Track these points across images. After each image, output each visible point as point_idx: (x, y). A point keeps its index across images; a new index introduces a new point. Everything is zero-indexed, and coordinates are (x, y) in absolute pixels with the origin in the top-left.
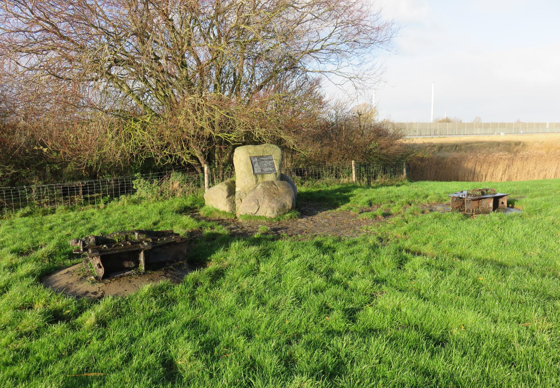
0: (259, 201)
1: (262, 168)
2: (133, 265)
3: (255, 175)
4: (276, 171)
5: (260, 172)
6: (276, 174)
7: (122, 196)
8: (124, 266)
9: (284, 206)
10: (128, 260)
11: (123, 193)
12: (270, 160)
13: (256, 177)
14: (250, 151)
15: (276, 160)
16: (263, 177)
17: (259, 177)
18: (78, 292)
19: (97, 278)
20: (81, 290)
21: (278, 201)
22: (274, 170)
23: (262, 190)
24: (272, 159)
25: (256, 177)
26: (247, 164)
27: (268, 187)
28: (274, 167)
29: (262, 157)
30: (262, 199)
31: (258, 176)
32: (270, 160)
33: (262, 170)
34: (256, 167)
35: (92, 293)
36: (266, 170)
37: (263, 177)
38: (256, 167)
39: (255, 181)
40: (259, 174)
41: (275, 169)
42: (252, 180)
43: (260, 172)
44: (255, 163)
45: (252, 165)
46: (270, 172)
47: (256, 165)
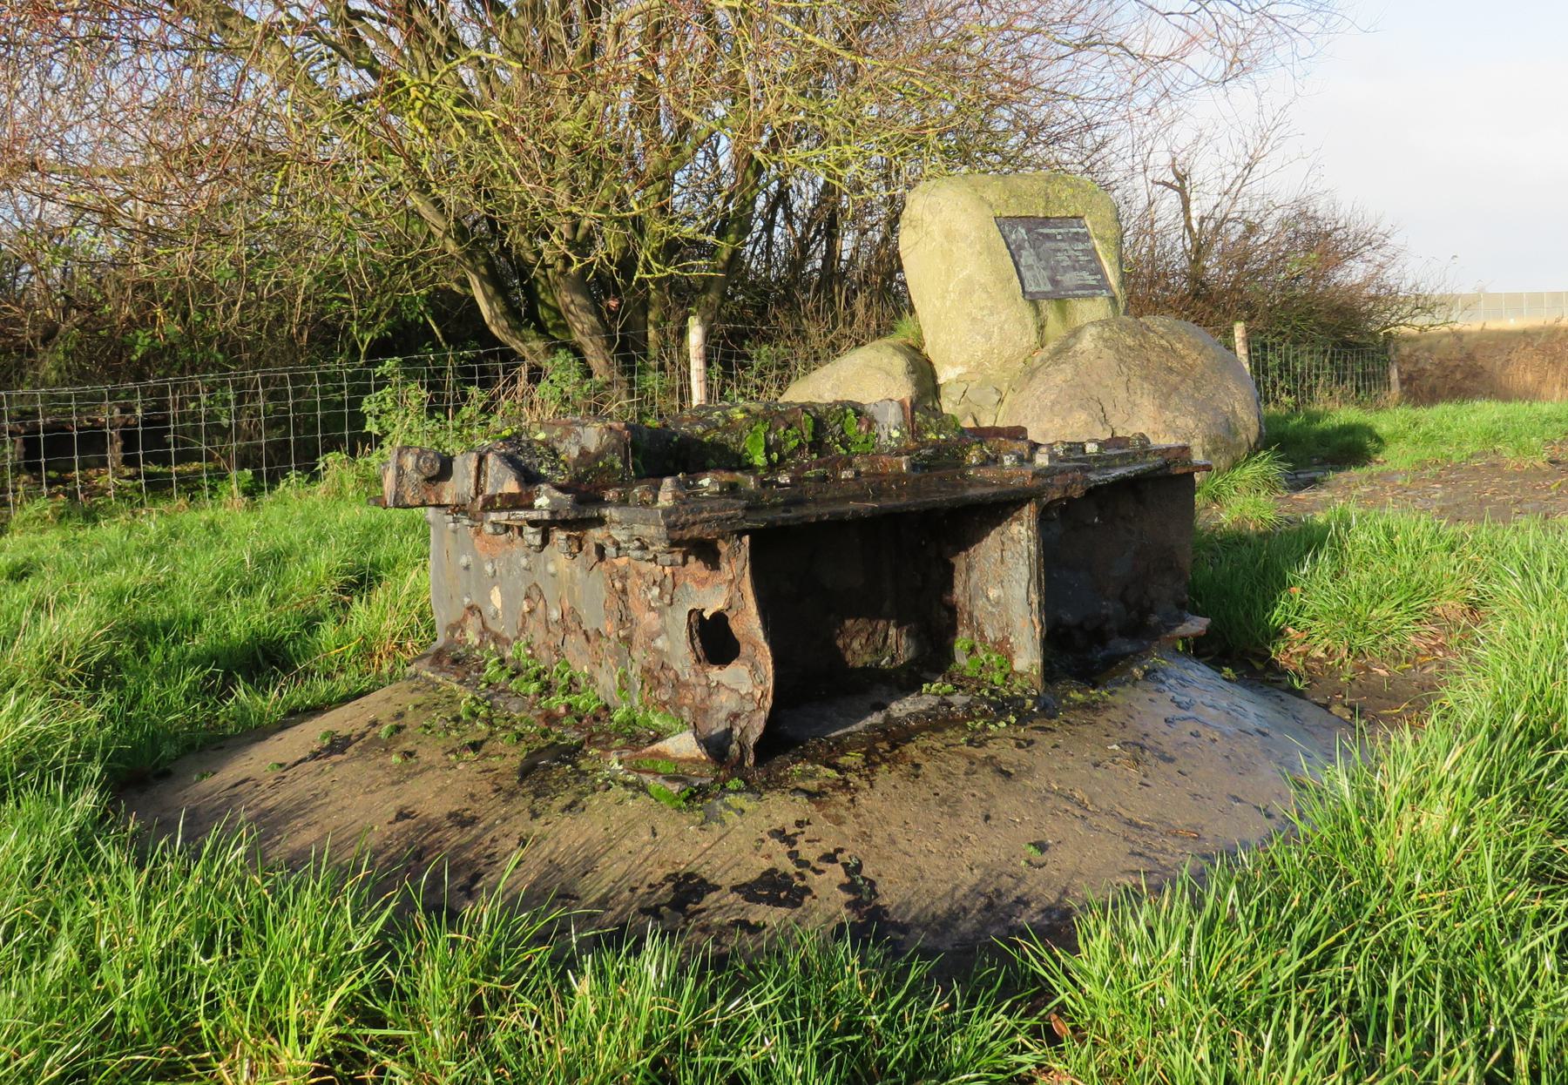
0: (1109, 408)
1: (1054, 270)
2: (899, 645)
3: (1033, 300)
4: (1109, 288)
5: (1049, 288)
6: (1113, 299)
7: (330, 457)
8: (838, 656)
9: (1230, 429)
10: (871, 610)
11: (332, 445)
12: (1077, 237)
13: (1038, 312)
14: (990, 196)
15: (1102, 239)
16: (1063, 312)
17: (1050, 311)
18: (593, 888)
19: (717, 747)
20: (611, 872)
21: (1201, 407)
22: (1103, 284)
23: (1108, 354)
24: (1087, 237)
25: (1038, 312)
26: (989, 248)
27: (1130, 341)
28: (1099, 270)
29: (1046, 220)
30: (1121, 394)
31: (1044, 304)
32: (1077, 237)
33: (1054, 282)
34: (1030, 267)
35: (749, 891)
36: (1070, 279)
37: (1063, 312)
38: (1030, 267)
39: (1032, 328)
40: (1046, 295)
41: (1104, 277)
42: (1021, 321)
43: (1049, 288)
44: (1020, 247)
45: (1013, 256)
46: (1090, 292)
47: (1027, 257)
